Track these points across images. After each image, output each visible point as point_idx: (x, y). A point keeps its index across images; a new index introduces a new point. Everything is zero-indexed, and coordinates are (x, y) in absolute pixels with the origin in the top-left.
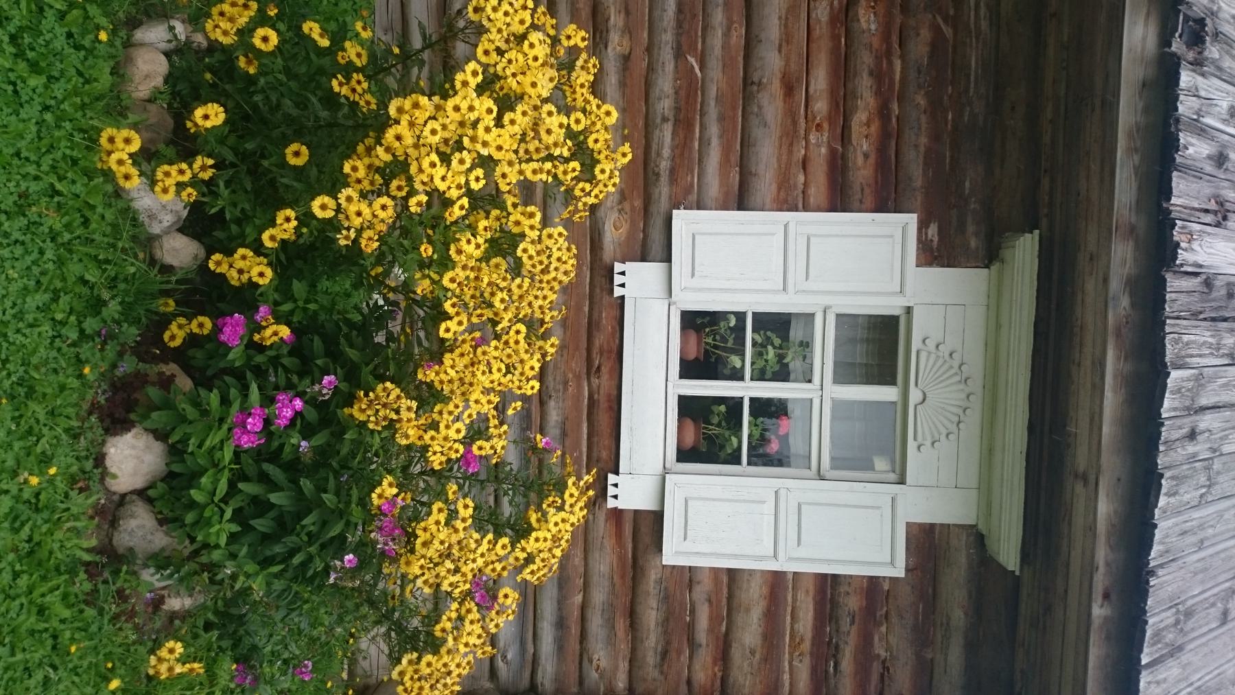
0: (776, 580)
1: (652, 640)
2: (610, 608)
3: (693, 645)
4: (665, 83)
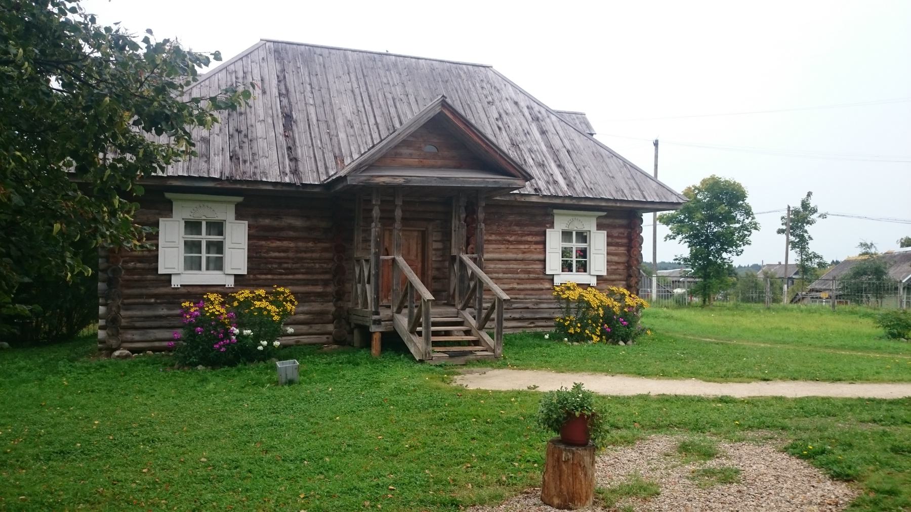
0: (608, 254)
1: (618, 277)
4: (522, 276)
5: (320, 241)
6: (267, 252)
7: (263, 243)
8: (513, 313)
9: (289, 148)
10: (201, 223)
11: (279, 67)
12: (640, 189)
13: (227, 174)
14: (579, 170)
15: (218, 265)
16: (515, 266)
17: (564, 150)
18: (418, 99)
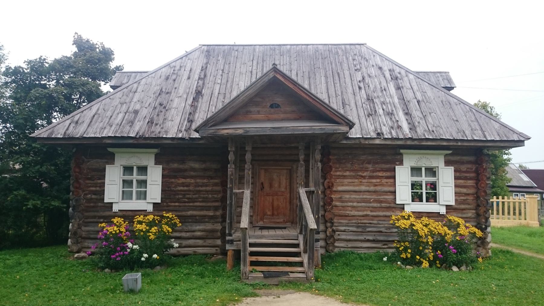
0: (456, 186)
2: (462, 213)
3: (467, 199)
4: (375, 205)
5: (212, 178)
6: (176, 187)
7: (173, 180)
8: (367, 235)
9: (190, 114)
10: (133, 168)
11: (205, 61)
12: (482, 129)
13: (141, 134)
14: (425, 117)
15: (142, 196)
16: (368, 197)
17: (415, 100)
18: (299, 72)
